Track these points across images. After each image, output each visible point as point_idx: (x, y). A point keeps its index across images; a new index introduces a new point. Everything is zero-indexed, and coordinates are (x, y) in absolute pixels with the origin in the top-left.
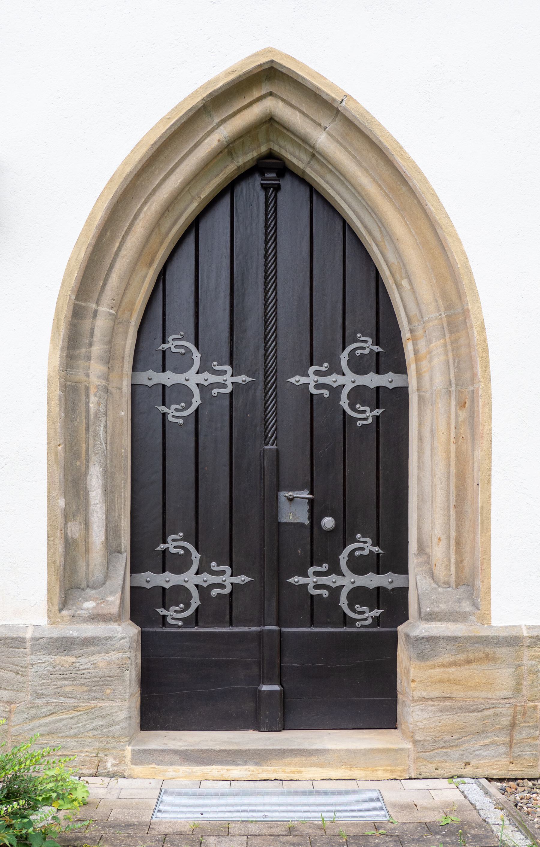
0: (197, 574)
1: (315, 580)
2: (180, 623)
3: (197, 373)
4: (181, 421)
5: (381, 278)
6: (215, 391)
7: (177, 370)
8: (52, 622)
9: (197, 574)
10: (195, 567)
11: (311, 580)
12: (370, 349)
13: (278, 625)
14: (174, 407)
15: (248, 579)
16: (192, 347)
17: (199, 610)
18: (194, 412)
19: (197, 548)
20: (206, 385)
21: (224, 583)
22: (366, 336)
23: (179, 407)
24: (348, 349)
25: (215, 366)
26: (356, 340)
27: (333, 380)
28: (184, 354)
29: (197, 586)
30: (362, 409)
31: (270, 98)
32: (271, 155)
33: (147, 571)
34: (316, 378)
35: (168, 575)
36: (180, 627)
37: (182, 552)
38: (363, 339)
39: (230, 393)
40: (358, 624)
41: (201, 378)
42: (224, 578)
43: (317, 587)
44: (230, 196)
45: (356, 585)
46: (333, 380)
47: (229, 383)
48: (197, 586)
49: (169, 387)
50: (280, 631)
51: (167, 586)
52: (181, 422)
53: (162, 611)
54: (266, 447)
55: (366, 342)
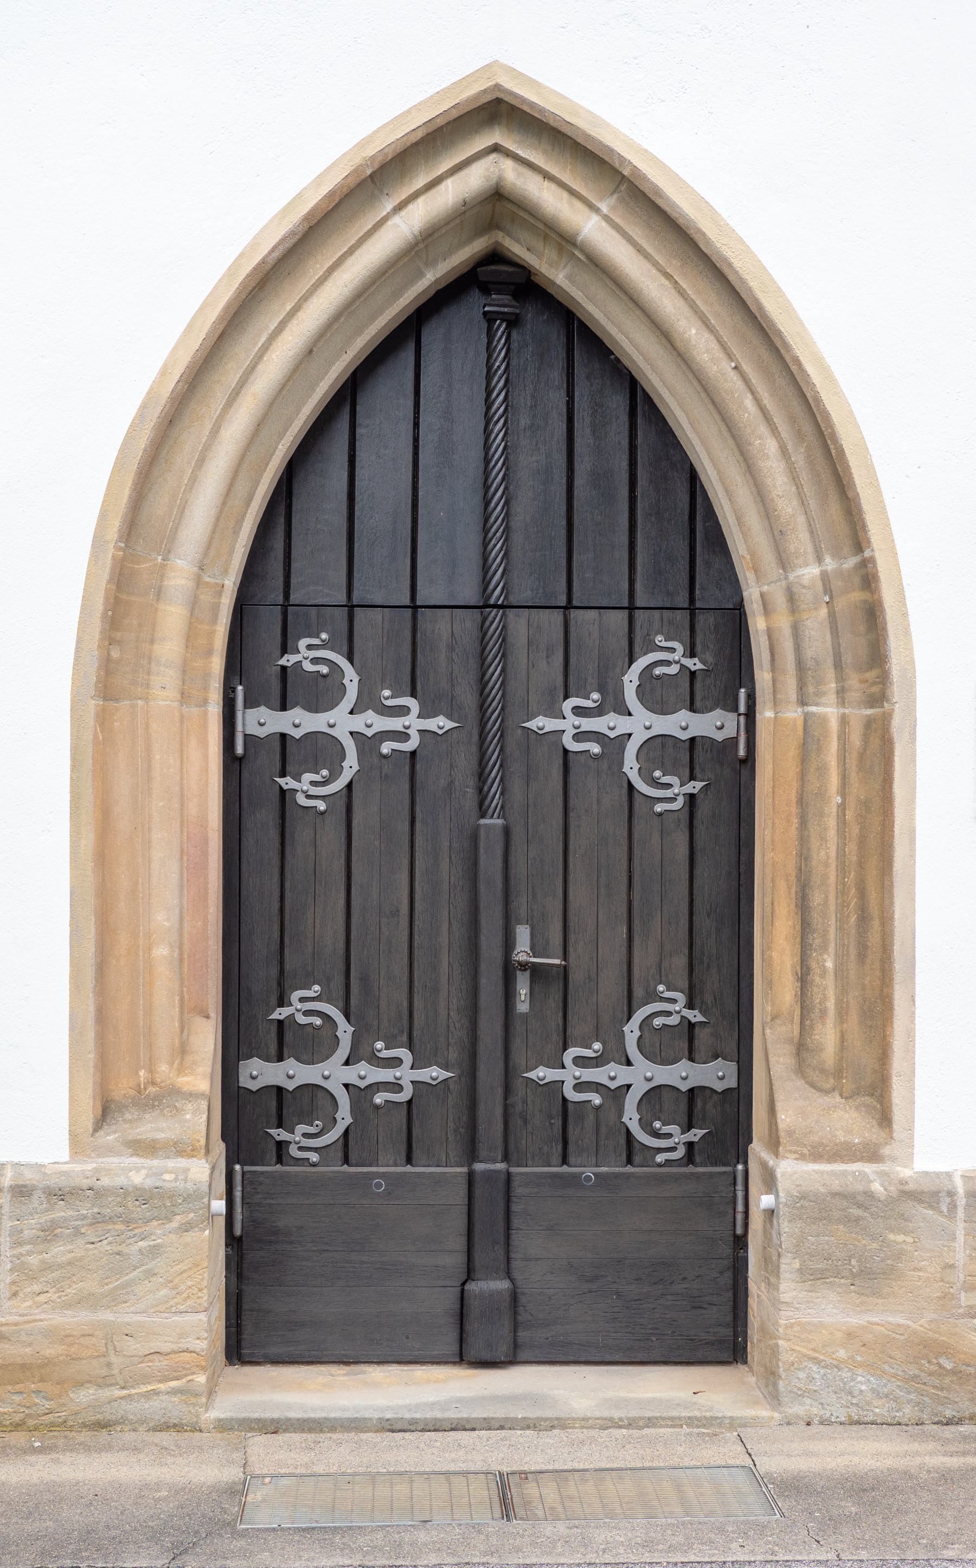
0: (347, 1063)
1: (577, 1074)
2: (314, 1157)
3: (351, 713)
4: (322, 806)
5: (702, 486)
6: (386, 747)
7: (314, 707)
8: (77, 1145)
9: (347, 1063)
10: (343, 1051)
11: (568, 724)
12: (682, 1017)
13: (506, 1158)
14: (301, 1128)
15: (450, 725)
16: (334, 1012)
17: (351, 1136)
18: (345, 790)
19: (347, 1016)
20: (370, 736)
21: (399, 1082)
22: (672, 640)
23: (317, 778)
24: (642, 662)
25: (387, 699)
26: (653, 997)
27: (609, 724)
28: (322, 813)
29: (346, 1086)
30: (666, 780)
31: (493, 157)
32: (495, 257)
33: (259, 706)
34: (577, 721)
35: (291, 1065)
36: (314, 1165)
37: (324, 670)
38: (668, 994)
39: (407, 1102)
40: (660, 1158)
41: (358, 723)
42: (406, 721)
43: (580, 1086)
44: (413, 345)
45: (655, 732)
46: (609, 724)
47: (406, 1083)
48: (346, 1086)
49: (291, 1092)
50: (508, 1170)
51: (290, 1086)
52: (315, 1160)
53: (281, 1134)
54: (482, 821)
55: (673, 1001)
